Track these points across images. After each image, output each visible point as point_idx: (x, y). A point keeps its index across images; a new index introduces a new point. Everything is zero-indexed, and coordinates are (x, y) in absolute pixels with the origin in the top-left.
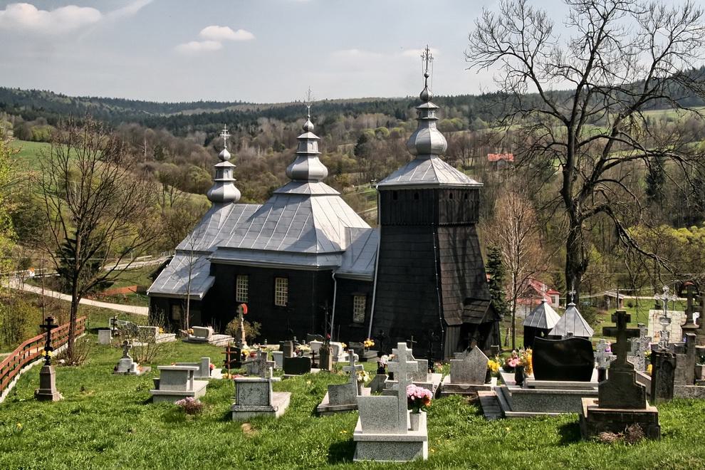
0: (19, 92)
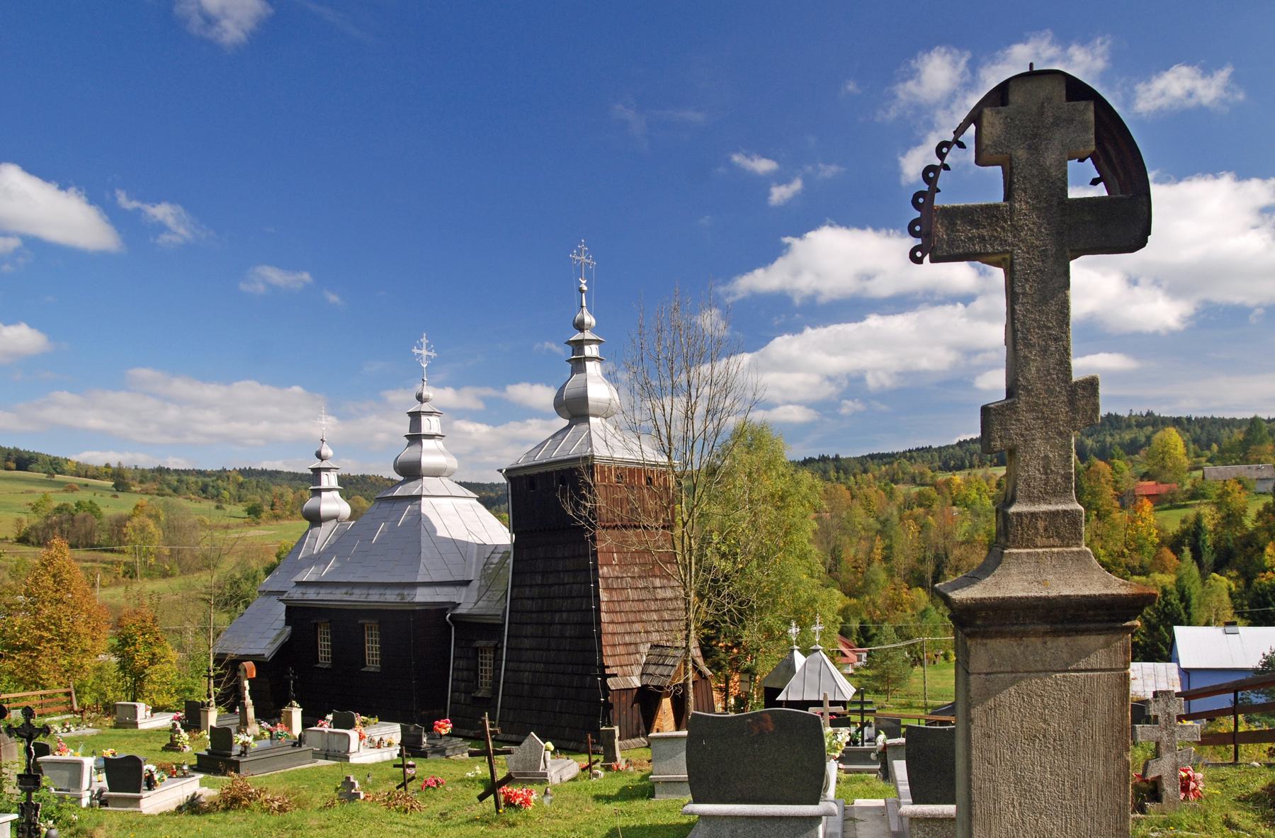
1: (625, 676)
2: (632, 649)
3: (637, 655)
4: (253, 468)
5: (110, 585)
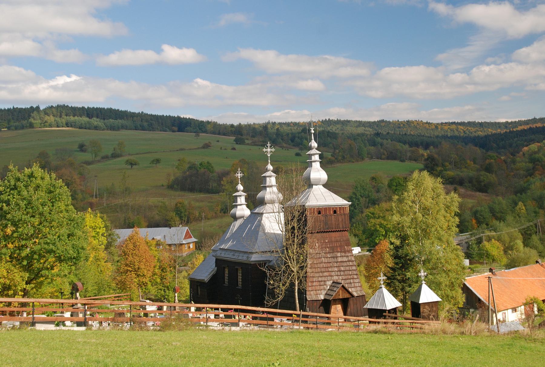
0: (398, 122)
1: (317, 294)
2: (322, 283)
3: (325, 286)
4: (331, 119)
5: (212, 218)
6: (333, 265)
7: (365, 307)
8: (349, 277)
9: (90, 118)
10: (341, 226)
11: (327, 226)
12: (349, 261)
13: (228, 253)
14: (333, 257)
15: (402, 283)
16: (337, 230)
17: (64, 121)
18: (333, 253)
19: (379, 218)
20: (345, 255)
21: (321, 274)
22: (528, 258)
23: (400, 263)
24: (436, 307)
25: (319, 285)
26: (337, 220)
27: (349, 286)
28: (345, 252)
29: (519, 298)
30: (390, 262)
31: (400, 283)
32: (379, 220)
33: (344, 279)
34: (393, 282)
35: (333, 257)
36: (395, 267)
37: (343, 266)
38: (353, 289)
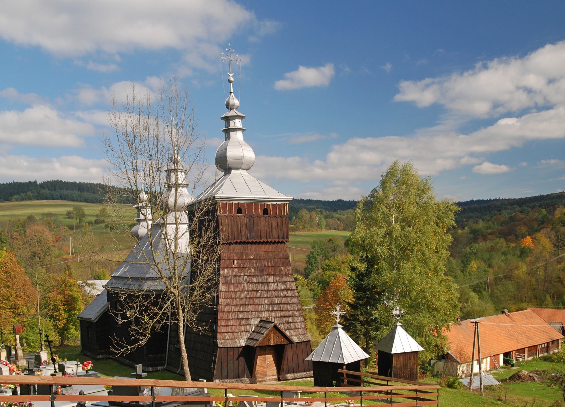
1: (235, 339)
2: (243, 322)
6: (261, 294)
7: (308, 358)
8: (287, 314)
9: (81, 192)
10: (275, 235)
11: (253, 234)
12: (287, 290)
13: (119, 282)
14: (262, 283)
15: (366, 326)
16: (269, 240)
17: (58, 194)
18: (261, 276)
19: (334, 269)
20: (281, 280)
21: (242, 308)
22: (484, 311)
23: (364, 298)
24: (415, 359)
25: (239, 325)
26: (269, 225)
27: (286, 328)
28: (281, 275)
29: (485, 349)
30: (349, 295)
31: (364, 325)
32: (334, 272)
33: (278, 317)
34: (352, 323)
35: (262, 283)
36: (357, 303)
37: (277, 297)
38: (292, 332)
